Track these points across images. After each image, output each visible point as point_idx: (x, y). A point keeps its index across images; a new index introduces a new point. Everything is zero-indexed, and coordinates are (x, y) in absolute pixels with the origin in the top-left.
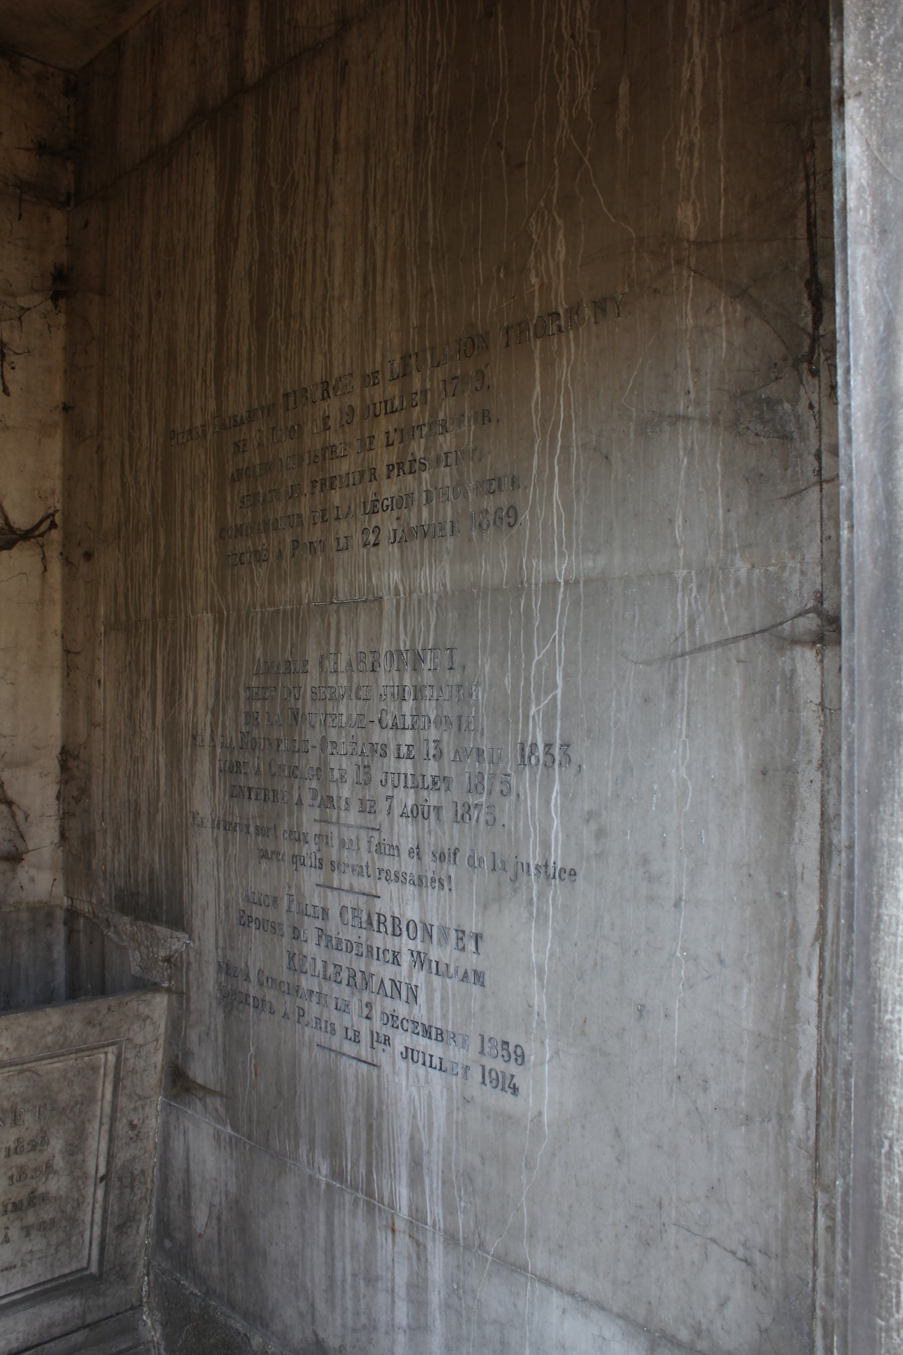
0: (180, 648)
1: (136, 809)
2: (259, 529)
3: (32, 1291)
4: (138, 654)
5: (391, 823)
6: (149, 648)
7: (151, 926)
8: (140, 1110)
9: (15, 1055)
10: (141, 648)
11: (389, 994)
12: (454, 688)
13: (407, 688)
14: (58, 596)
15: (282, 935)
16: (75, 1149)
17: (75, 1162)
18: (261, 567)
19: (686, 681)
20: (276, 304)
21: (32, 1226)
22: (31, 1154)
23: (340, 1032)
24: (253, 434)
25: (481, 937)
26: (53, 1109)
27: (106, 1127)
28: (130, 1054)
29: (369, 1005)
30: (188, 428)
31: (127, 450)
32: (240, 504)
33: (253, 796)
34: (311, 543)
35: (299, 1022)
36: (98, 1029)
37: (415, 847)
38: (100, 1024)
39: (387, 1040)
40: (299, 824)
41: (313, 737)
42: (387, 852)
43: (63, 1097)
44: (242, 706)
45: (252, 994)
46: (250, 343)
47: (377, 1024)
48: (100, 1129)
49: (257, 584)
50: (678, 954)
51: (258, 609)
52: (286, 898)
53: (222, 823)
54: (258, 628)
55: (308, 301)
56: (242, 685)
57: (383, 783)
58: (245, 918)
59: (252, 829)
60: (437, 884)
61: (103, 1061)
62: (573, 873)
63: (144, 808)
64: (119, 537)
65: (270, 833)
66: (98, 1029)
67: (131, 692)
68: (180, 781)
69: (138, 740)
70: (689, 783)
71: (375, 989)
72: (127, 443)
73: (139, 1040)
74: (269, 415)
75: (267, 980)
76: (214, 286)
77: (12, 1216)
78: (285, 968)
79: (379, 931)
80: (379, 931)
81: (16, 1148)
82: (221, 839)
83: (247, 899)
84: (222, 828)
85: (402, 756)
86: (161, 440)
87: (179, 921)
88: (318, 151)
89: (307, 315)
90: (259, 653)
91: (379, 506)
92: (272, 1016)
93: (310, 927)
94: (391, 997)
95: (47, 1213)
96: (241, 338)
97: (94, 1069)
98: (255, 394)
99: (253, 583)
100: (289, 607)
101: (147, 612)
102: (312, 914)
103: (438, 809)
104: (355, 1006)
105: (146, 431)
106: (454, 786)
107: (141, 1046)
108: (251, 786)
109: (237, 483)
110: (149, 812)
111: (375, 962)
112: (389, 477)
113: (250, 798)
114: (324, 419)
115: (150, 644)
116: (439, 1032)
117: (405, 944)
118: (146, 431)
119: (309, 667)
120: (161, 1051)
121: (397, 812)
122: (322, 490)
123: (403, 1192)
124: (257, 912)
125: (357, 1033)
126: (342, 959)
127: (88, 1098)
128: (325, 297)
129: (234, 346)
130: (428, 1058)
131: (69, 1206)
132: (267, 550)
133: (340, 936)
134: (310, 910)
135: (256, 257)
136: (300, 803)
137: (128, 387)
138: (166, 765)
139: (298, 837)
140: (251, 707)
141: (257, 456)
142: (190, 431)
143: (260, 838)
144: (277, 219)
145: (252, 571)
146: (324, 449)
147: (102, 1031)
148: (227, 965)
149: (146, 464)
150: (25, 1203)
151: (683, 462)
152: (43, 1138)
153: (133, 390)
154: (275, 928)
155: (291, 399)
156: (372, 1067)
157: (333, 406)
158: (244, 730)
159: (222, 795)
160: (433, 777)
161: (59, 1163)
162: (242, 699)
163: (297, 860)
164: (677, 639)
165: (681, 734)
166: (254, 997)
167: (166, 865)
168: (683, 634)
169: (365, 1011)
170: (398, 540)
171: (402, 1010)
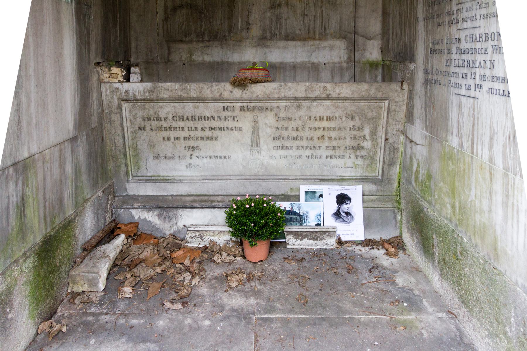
3: (359, 178)
9: (351, 96)
11: (483, 67)
16: (373, 133)
22: (358, 132)
23: (464, 87)
27: (384, 129)
28: (393, 104)
29: (475, 73)
43: (369, 115)
47: (478, 81)
73: (397, 99)
75: (439, 72)
95: (364, 153)
97: (381, 108)
120: (405, 105)
123: (486, 151)
124: (437, 47)
127: (379, 117)
139: (450, 13)
147: (383, 94)
161: (368, 137)
163: (451, 23)
171: (488, 72)
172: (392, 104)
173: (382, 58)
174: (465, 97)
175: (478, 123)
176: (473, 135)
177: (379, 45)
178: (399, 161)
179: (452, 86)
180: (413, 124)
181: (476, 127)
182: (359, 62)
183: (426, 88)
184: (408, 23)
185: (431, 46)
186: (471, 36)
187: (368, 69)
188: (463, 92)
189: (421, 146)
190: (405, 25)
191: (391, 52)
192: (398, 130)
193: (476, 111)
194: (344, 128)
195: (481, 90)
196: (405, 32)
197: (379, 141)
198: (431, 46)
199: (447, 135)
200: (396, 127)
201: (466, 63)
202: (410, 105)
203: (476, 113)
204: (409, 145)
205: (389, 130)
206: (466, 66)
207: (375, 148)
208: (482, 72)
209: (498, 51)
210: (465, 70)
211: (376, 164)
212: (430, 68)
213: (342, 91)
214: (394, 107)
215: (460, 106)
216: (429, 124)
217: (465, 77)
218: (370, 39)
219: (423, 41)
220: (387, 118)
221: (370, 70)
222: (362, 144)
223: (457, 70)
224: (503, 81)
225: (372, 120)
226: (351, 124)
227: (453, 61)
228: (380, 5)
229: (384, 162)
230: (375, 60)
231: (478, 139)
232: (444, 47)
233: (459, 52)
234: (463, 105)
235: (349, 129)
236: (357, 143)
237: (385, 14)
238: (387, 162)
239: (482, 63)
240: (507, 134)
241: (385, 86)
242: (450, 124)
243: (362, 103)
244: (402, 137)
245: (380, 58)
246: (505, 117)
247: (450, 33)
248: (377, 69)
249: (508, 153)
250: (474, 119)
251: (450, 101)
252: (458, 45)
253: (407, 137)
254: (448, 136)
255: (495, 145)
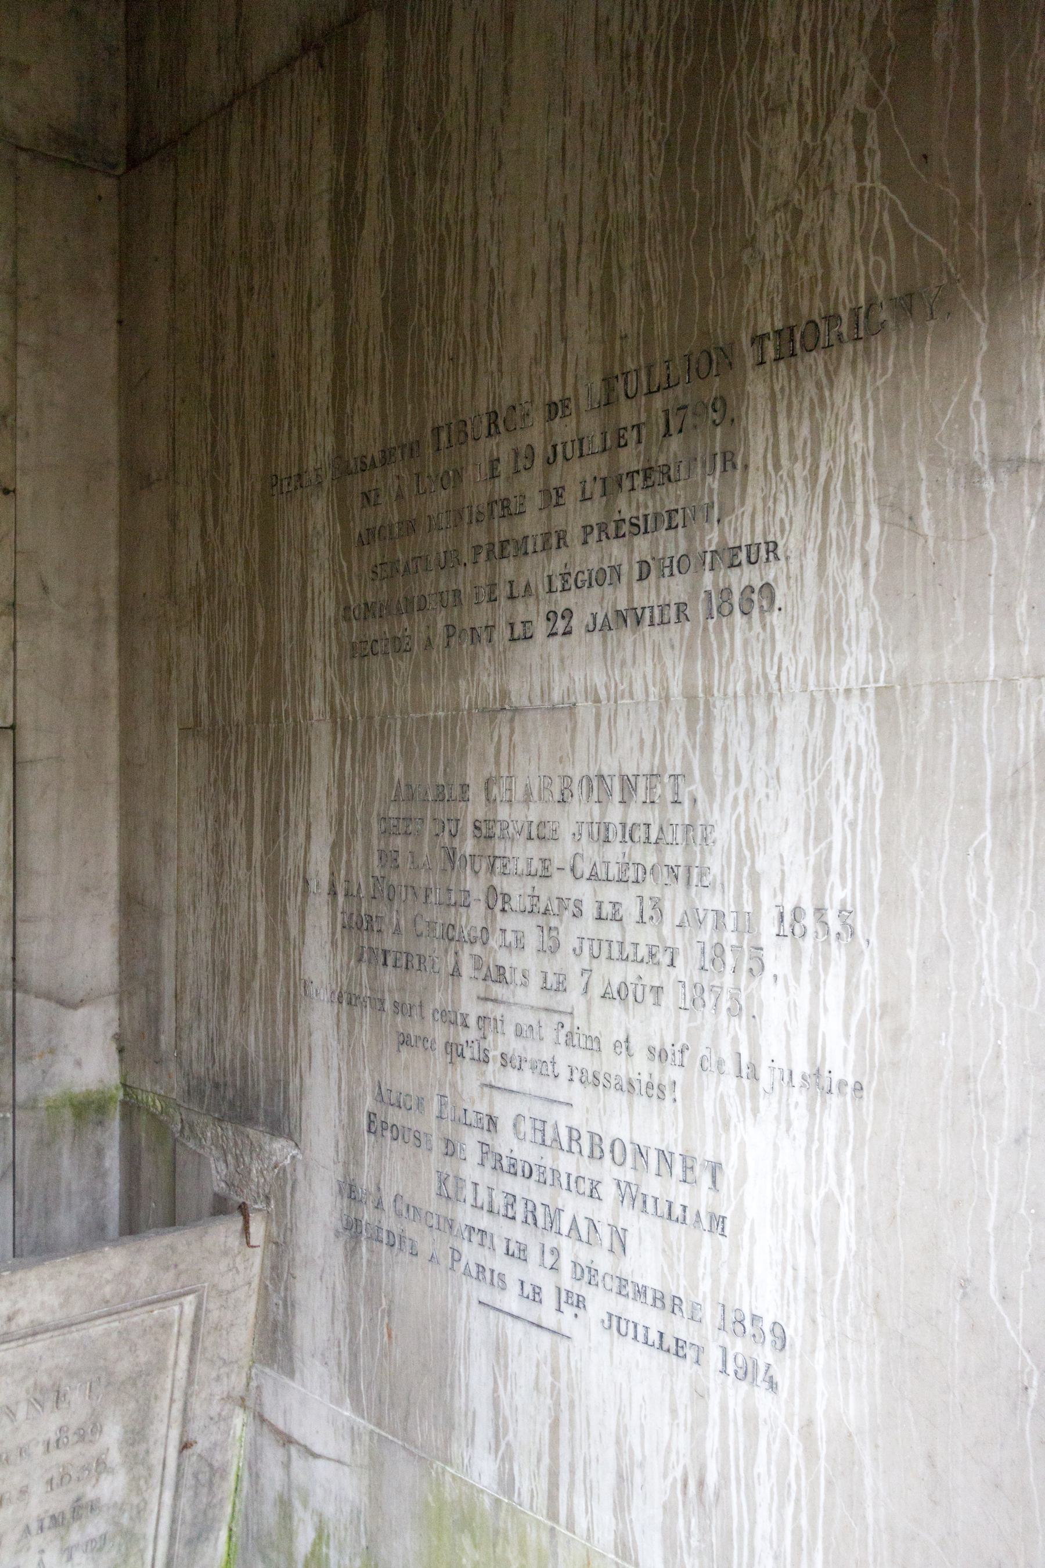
0: (287, 766)
1: (223, 972)
2: (398, 610)
4: (227, 767)
5: (589, 1003)
6: (242, 761)
7: (241, 1128)
8: (225, 1379)
10: (232, 761)
11: (584, 1238)
12: (680, 829)
13: (611, 827)
14: (114, 690)
15: (430, 1150)
16: (136, 1436)
17: (136, 1455)
18: (401, 659)
19: (1032, 830)
20: (421, 305)
21: (77, 1546)
22: (78, 1448)
24: (390, 481)
25: (721, 1168)
26: (109, 1384)
27: (178, 1406)
30: (295, 471)
31: (209, 498)
32: (371, 575)
33: (390, 962)
34: (473, 629)
35: (452, 1268)
36: (172, 1273)
37: (622, 1039)
38: (176, 1266)
39: (580, 1303)
40: (456, 1001)
41: (475, 885)
42: (582, 1044)
44: (375, 842)
45: (385, 1227)
46: (383, 358)
47: (567, 1282)
48: (170, 1407)
49: (396, 681)
50: (1022, 1211)
51: (398, 715)
52: (436, 1098)
53: (345, 996)
54: (398, 740)
55: (467, 303)
56: (375, 813)
57: (577, 953)
58: (378, 1123)
59: (388, 1005)
60: (656, 1090)
61: (177, 1315)
62: (858, 1087)
63: (234, 969)
64: (200, 614)
65: (414, 1012)
66: (172, 1273)
67: (217, 820)
68: (287, 938)
69: (226, 882)
70: (1037, 972)
71: (565, 1230)
72: (209, 490)
73: (226, 1284)
74: (411, 456)
76: (329, 282)
77: (50, 1534)
78: (433, 1195)
79: (570, 1151)
80: (570, 1151)
81: (58, 1441)
82: (344, 1017)
83: (380, 1098)
84: (344, 1004)
85: (604, 916)
86: (258, 487)
87: (282, 1123)
88: (478, 93)
89: (466, 319)
90: (398, 773)
91: (571, 581)
92: (414, 1259)
93: (470, 1141)
94: (588, 1243)
95: (96, 1526)
96: (371, 351)
97: (165, 1326)
98: (391, 427)
99: (390, 680)
100: (441, 714)
101: (238, 714)
102: (474, 1123)
103: (658, 990)
104: (534, 1253)
105: (235, 474)
106: (679, 961)
107: (229, 1292)
108: (386, 947)
109: (367, 547)
110: (242, 978)
111: (565, 1194)
112: (585, 543)
113: (385, 964)
114: (491, 462)
115: (245, 756)
116: (658, 1295)
117: (607, 1172)
118: (235, 474)
119: (470, 794)
120: (255, 1297)
121: (597, 990)
122: (488, 559)
124: (395, 1117)
125: (537, 1290)
126: (516, 1185)
127: (158, 1365)
128: (491, 294)
129: (361, 361)
130: (641, 1331)
131: (126, 1515)
132: (409, 637)
133: (515, 1155)
134: (471, 1117)
135: (391, 239)
136: (456, 973)
137: (210, 416)
138: (267, 917)
139: (452, 1018)
140: (387, 844)
141: (395, 512)
142: (299, 475)
143: (399, 1018)
144: (420, 186)
145: (388, 665)
146: (491, 503)
147: (178, 1275)
148: (351, 1186)
149: (237, 519)
150: (68, 1516)
151: (1029, 524)
152: (95, 1425)
153: (216, 420)
154: (418, 1139)
155: (444, 436)
156: (559, 1338)
157: (502, 447)
158: (377, 874)
159: (346, 958)
160: (650, 947)
161: (115, 1457)
162: (375, 832)
163: (454, 1051)
164: (1017, 771)
165: (1023, 903)
166: (389, 1232)
167: (265, 1049)
168: (1026, 764)
169: (549, 1260)
170: (598, 627)
171: (604, 1262)
172: (211, 1306)
173: (124, 1076)
174: (519, 1326)
175: (572, 1421)
176: (555, 1457)
177: (108, 1024)
178: (229, 1510)
179: (467, 1273)
180: (291, 1374)
181: (564, 1431)
182: (32, 1105)
183: (351, 1253)
184: (255, 974)
185: (369, 1103)
186: (538, 1125)
187: (69, 1127)
188: (511, 1301)
189: (333, 1465)
190: (245, 986)
191: (172, 1067)
192: (229, 1397)
193: (564, 1377)
194: (22, 1451)
195: (581, 1313)
196: (244, 1011)
197: (156, 1458)
198: (369, 1103)
199: (447, 1442)
200: (219, 1390)
201: (520, 1207)
202: (275, 1299)
203: (563, 1385)
204: (272, 1454)
205: (198, 1407)
206: (520, 1217)
207: (139, 1491)
208: (584, 1255)
209: (730, 1317)
210: (518, 1232)
211: (142, 1552)
212: (366, 1182)
213: (22, 1304)
214: (215, 1315)
215: (499, 1350)
216: (369, 1387)
217: (518, 1253)
218: (74, 1006)
219: (334, 1074)
220: (191, 1361)
221: (77, 1133)
222: (91, 1494)
223: (484, 1221)
224: (659, 1303)
225: (134, 1384)
226: (51, 1423)
227: (469, 1187)
228: (112, 864)
229: (172, 1536)
230: (93, 1087)
231: (572, 1472)
232: (428, 1123)
233: (490, 1163)
234: (513, 1350)
235: (41, 1448)
236: (72, 1496)
237: (134, 906)
238: (184, 1532)
239: (583, 1226)
240: (678, 1473)
241: (189, 1244)
242: (460, 1402)
243: (97, 1329)
244: (239, 1419)
245: (113, 1078)
246: (667, 1418)
247: (453, 1085)
248: (101, 1123)
249: (683, 1534)
250: (557, 1404)
251: (461, 1324)
252: (486, 1137)
253: (261, 1419)
254: (455, 1447)
255: (637, 1501)
